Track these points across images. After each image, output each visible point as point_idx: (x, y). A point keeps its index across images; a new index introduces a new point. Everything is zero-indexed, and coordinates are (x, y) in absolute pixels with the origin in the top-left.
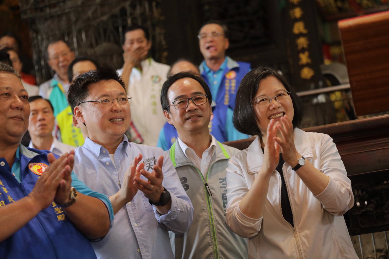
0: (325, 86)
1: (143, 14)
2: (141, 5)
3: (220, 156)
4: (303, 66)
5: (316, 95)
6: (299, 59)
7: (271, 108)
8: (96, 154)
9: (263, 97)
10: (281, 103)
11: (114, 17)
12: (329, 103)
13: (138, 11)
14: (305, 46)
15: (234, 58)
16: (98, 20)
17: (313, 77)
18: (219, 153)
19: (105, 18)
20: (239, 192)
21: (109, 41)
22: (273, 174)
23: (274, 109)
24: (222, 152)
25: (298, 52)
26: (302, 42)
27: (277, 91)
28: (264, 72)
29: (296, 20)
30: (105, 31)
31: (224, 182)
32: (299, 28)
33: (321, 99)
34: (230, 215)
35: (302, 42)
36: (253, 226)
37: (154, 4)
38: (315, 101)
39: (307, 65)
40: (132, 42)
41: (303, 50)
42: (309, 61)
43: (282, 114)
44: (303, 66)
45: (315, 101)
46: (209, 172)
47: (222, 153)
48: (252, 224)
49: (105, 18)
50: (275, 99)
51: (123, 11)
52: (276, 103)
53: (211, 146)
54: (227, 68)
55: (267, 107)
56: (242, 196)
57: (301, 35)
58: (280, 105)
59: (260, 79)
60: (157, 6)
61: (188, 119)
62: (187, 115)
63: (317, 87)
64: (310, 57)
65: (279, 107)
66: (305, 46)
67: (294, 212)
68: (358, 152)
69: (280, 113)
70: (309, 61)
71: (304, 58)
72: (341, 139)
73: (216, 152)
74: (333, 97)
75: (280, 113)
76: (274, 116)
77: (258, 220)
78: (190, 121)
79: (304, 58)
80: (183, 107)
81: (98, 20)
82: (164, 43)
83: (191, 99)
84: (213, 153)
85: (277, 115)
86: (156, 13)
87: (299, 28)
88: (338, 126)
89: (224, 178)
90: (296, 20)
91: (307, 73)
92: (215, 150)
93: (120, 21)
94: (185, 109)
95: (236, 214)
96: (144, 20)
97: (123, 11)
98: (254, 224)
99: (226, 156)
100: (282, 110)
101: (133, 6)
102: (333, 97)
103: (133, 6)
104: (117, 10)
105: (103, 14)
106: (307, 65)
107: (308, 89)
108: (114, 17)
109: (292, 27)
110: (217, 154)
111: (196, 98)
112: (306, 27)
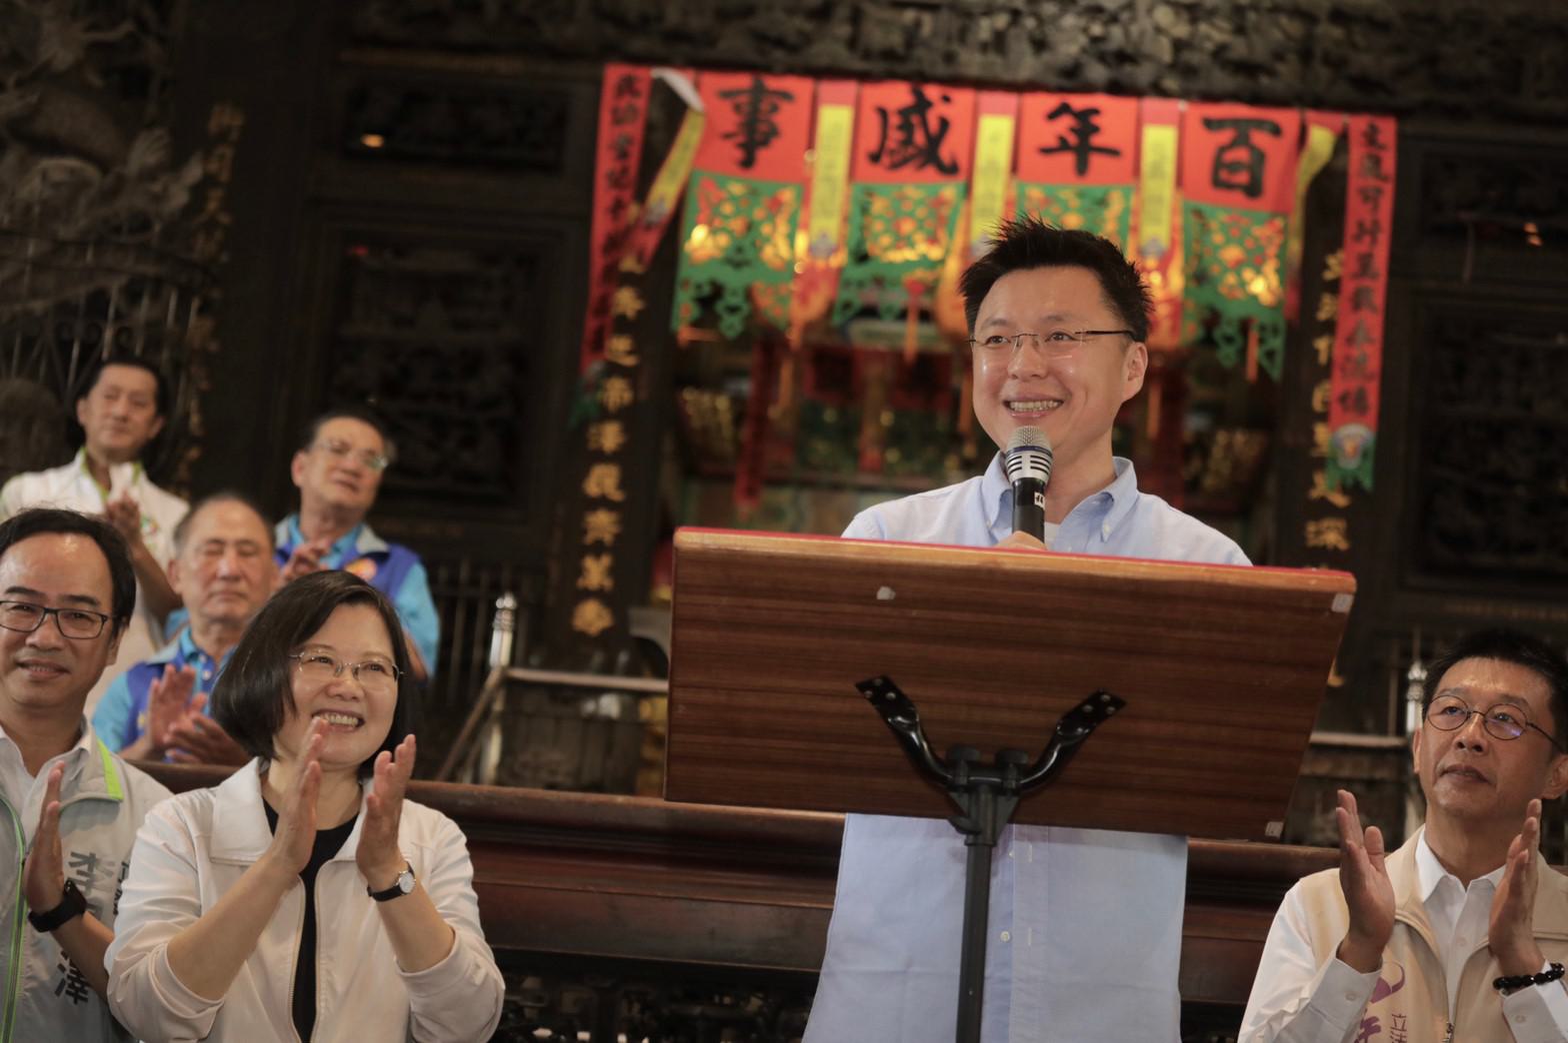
0: (632, 671)
1: (154, 325)
2: (156, 296)
3: (91, 788)
4: (587, 594)
5: (597, 692)
6: (580, 571)
7: (334, 690)
8: (1549, 734)
9: (321, 652)
10: (364, 691)
11: (65, 309)
12: (631, 723)
13: (144, 311)
14: (608, 538)
15: (380, 534)
16: (18, 307)
17: (605, 634)
18: (92, 778)
19: (38, 306)
20: (165, 909)
21: (33, 375)
22: (291, 885)
23: (341, 697)
24: (103, 776)
25: (579, 549)
26: (602, 524)
27: (369, 654)
28: (353, 587)
29: (601, 457)
30: (28, 344)
31: (84, 868)
32: (603, 480)
33: (610, 706)
34: (129, 970)
35: (602, 524)
36: (195, 1019)
37: (195, 304)
38: (589, 707)
39: (599, 594)
40: (113, 395)
41: (598, 549)
42: (608, 583)
43: (355, 721)
44: (587, 594)
45: (589, 707)
46: (444, 866)
47: (103, 779)
48: (191, 1011)
49: (38, 306)
50: (356, 672)
51: (98, 303)
52: (349, 683)
53: (76, 748)
54: (353, 548)
55: (323, 684)
56: (177, 923)
57: (603, 502)
58: (360, 693)
59: (337, 604)
60: (201, 311)
61: (23, 665)
62: (24, 655)
63: (608, 669)
64: (612, 571)
65: (355, 698)
66: (608, 538)
67: (323, 1011)
68: (660, 894)
69: (351, 715)
70: (608, 583)
71: (595, 572)
72: (488, 833)
73: (84, 773)
74: (646, 710)
75: (351, 715)
76: (330, 715)
77: (213, 1005)
78: (25, 673)
79: (595, 572)
80: (24, 623)
81: (18, 307)
82: (195, 419)
83: (55, 612)
84: (75, 770)
85: (339, 717)
86: (198, 326)
87: (603, 480)
88: (622, 807)
89: (88, 855)
90: (601, 457)
91: (592, 617)
92: (83, 764)
93: (79, 327)
94: (29, 633)
95: (152, 972)
96: (154, 343)
97: (98, 303)
98: (199, 1012)
99: (114, 791)
100: (356, 708)
101: (133, 294)
102: (646, 710)
103: (133, 294)
104: (80, 293)
105: (34, 294)
106: (599, 594)
107: (578, 666)
108: (65, 309)
109: (584, 474)
110: (84, 777)
111: (73, 610)
112: (623, 484)
